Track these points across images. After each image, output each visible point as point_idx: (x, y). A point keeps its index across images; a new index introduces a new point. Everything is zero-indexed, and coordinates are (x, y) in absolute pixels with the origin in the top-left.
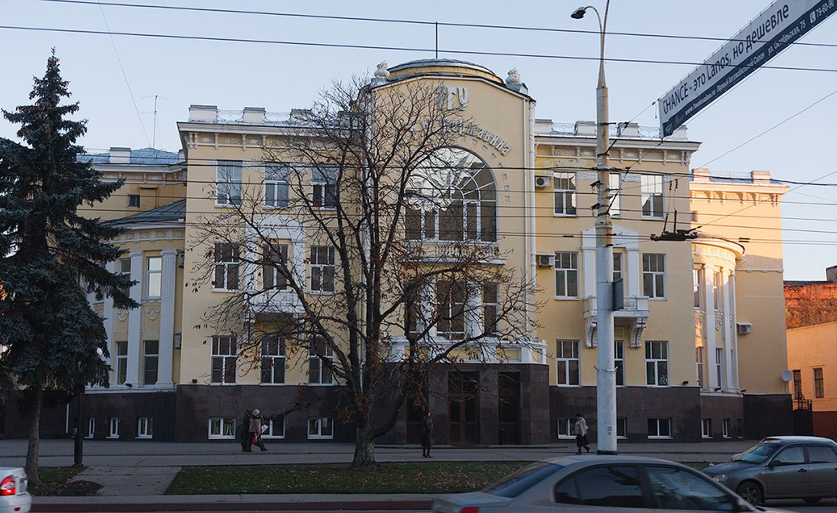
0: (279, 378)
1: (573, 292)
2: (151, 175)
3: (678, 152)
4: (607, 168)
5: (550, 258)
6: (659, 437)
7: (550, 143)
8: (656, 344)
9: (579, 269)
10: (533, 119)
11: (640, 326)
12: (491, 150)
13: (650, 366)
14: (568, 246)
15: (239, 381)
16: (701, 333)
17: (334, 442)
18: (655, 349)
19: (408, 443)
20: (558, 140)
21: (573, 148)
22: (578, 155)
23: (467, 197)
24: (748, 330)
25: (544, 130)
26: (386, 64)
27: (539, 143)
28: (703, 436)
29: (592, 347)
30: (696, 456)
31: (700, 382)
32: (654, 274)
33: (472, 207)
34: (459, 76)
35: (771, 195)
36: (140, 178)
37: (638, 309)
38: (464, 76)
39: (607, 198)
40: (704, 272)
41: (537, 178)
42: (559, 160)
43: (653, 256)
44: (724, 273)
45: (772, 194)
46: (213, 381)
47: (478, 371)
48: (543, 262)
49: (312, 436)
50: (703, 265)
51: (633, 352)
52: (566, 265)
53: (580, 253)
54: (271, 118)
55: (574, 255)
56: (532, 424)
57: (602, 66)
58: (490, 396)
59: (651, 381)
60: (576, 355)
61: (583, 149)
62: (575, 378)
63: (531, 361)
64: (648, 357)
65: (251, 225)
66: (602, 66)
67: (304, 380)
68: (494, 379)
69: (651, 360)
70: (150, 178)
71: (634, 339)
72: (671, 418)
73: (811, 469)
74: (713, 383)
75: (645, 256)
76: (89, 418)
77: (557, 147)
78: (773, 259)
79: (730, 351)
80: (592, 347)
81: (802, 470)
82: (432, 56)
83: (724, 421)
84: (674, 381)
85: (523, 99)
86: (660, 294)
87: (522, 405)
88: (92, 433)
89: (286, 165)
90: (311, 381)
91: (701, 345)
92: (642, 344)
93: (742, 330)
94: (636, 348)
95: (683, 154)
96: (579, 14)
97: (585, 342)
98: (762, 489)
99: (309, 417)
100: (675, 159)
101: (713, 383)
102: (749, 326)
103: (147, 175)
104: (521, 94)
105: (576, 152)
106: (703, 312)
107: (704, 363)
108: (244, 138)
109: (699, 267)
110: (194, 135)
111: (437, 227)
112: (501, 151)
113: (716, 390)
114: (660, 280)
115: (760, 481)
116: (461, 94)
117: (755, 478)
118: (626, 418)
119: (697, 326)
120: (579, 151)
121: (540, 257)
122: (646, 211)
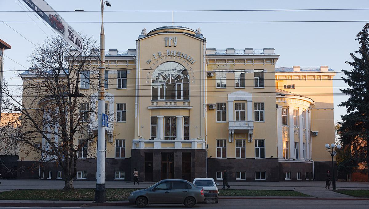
0: (263, 155)
1: (224, 119)
3: (270, 59)
4: (102, 67)
5: (213, 106)
6: (260, 179)
7: (214, 58)
8: (260, 140)
9: (246, 110)
10: (205, 49)
11: (250, 133)
12: (187, 62)
13: (257, 150)
14: (222, 100)
15: (228, 157)
16: (287, 136)
17: (266, 181)
18: (260, 143)
19: (145, 181)
21: (225, 60)
22: (227, 63)
23: (178, 82)
24: (317, 134)
25: (213, 53)
26: (146, 29)
27: (208, 58)
29: (231, 142)
30: (287, 187)
32: (259, 111)
33: (179, 86)
34: (174, 33)
35: (329, 76)
37: (249, 126)
38: (176, 33)
39: (102, 80)
40: (289, 110)
41: (208, 73)
43: (259, 104)
44: (300, 110)
45: (320, 75)
46: (116, 157)
48: (210, 107)
49: (218, 178)
50: (288, 107)
51: (249, 144)
52: (221, 108)
53: (227, 103)
54: (236, 52)
55: (225, 104)
56: (196, 174)
58: (178, 162)
59: (238, 156)
60: (225, 145)
61: (228, 60)
62: (224, 154)
63: (196, 148)
64: (256, 146)
65: (9, 95)
68: (180, 155)
71: (250, 138)
73: (171, 192)
74: (292, 156)
75: (255, 104)
76: (57, 171)
77: (217, 60)
78: (329, 104)
79: (294, 144)
80: (231, 142)
81: (167, 192)
82: (171, 25)
83: (306, 173)
84: (267, 156)
85: (200, 40)
86: (262, 119)
87: (191, 166)
88: (50, 177)
90: (116, 157)
91: (287, 141)
92: (253, 141)
93: (314, 135)
94: (251, 142)
95: (272, 60)
96: (108, 4)
97: (228, 140)
98: (147, 200)
99: (236, 171)
100: (269, 63)
101: (292, 156)
102: (317, 132)
104: (200, 39)
105: (226, 61)
106: (288, 127)
107: (288, 148)
108: (254, 60)
109: (286, 108)
111: (165, 94)
112: (192, 62)
114: (262, 113)
115: (195, 198)
116: (174, 39)
117: (145, 195)
118: (290, 172)
119: (285, 133)
120: (117, 62)
121: (209, 106)
122: (237, 85)
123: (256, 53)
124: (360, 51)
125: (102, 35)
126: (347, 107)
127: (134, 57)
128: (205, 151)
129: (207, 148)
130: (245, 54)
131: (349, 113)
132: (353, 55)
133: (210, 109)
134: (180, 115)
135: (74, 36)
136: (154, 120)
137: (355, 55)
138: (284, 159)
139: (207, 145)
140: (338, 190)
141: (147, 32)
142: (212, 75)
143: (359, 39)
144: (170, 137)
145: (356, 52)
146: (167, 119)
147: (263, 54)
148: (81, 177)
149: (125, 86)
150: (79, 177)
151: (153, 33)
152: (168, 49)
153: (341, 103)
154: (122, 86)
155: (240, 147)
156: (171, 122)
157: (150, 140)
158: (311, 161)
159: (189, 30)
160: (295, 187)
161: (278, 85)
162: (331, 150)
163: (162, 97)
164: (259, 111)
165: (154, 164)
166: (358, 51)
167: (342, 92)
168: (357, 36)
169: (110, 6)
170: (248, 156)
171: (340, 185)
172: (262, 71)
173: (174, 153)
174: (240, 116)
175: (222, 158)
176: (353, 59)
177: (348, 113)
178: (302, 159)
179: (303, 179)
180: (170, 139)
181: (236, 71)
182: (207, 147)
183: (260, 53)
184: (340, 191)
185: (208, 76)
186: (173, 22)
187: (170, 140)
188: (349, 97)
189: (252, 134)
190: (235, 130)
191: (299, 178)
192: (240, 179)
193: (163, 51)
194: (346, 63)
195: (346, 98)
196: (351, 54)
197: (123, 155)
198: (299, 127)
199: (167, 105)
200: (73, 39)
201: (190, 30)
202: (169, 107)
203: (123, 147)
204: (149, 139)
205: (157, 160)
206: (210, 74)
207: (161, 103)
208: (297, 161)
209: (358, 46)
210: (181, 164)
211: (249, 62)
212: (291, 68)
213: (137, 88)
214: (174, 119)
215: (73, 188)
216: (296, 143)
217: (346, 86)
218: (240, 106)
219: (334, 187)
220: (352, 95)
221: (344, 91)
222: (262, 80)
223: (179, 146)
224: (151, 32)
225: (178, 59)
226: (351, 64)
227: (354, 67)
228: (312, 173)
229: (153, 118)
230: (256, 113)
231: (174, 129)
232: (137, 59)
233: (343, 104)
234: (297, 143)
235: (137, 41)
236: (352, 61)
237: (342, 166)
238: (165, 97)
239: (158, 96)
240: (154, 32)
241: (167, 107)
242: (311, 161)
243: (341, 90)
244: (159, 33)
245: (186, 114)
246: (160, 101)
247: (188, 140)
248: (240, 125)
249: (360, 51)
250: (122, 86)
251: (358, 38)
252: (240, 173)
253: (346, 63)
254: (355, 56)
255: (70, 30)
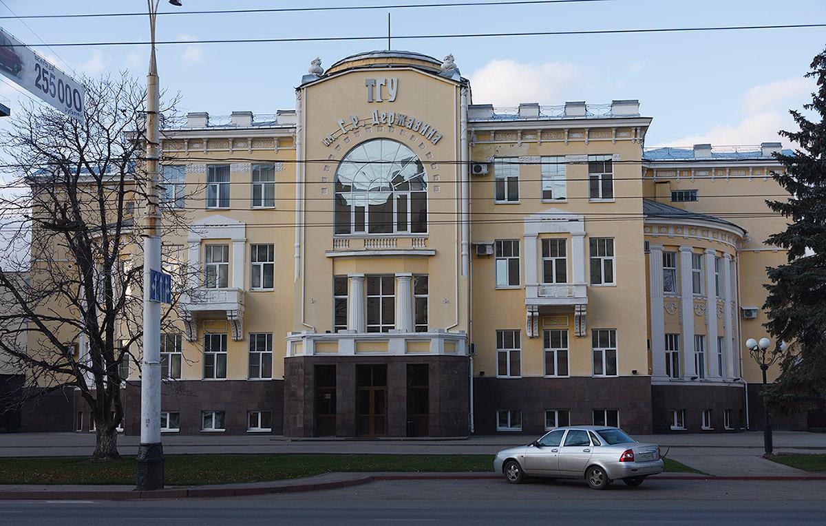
0: (563, 369)
2: (698, 171)
5: (487, 247)
6: (509, 429)
13: (668, 355)
20: (569, 122)
28: (704, 427)
29: (532, 337)
31: (650, 372)
32: (603, 259)
36: (674, 173)
38: (392, 67)
41: (474, 166)
42: (500, 145)
46: (206, 377)
47: (386, 363)
54: (544, 113)
57: (153, 48)
66: (153, 48)
67: (244, 376)
69: (551, 349)
70: (697, 173)
72: (684, 410)
80: (532, 337)
82: (382, 46)
89: (164, 160)
90: (251, 376)
99: (545, 410)
101: (688, 367)
103: (695, 171)
110: (636, 130)
113: (693, 378)
114: (609, 264)
123: (594, 112)
124: (817, 104)
125: (153, 75)
126: (786, 246)
127: (290, 130)
128: (465, 360)
129: (473, 352)
130: (566, 116)
131: (792, 261)
132: (797, 115)
133: (478, 255)
134: (402, 272)
135: (56, 82)
136: (341, 285)
137: (801, 115)
138: (668, 379)
139: (473, 345)
140: (780, 455)
141: (325, 66)
142: (484, 170)
143: (814, 73)
144: (381, 325)
145: (806, 107)
146: (371, 282)
147: (612, 115)
148: (258, 427)
149: (225, 201)
150: (504, 422)
151: (338, 69)
152: (375, 108)
153: (772, 236)
154: (218, 201)
155: (555, 350)
156: (379, 286)
157: (329, 334)
158: (739, 383)
159: (427, 59)
160: (669, 446)
161: (655, 194)
162: (761, 355)
163: (360, 227)
164: (603, 259)
165: (339, 394)
166: (812, 105)
167: (771, 210)
168: (812, 66)
169: (180, 5)
170: (572, 372)
171: (785, 441)
172: (607, 158)
173: (387, 365)
174: (555, 272)
175: (559, 377)
176: (798, 124)
177: (789, 260)
178: (713, 377)
179: (718, 429)
180: (381, 331)
181: (545, 160)
182: (472, 348)
183: (558, 113)
184: (783, 459)
185: (474, 172)
186: (389, 38)
187: (381, 334)
188: (790, 220)
189: (584, 316)
190: (541, 308)
191: (707, 425)
192: (259, 429)
193: (368, 113)
194: (780, 134)
195: (782, 223)
196: (791, 112)
197: (267, 372)
198: (681, 295)
199: (379, 246)
200: (51, 87)
201: (430, 60)
202: (377, 253)
203: (266, 352)
204: (327, 332)
205: (397, 386)
206: (478, 169)
207: (358, 241)
208: (701, 381)
209: (813, 87)
210: (404, 392)
211: (575, 135)
212: (688, 149)
213: (464, 202)
214: (389, 282)
215: (118, 453)
216: (700, 338)
217: (784, 196)
218: (553, 247)
219: (769, 446)
220: (797, 216)
221: (776, 206)
222: (608, 181)
223: (396, 348)
224: (333, 67)
225: (396, 132)
226: (792, 137)
227: (802, 146)
228: (742, 412)
229: (558, 279)
230: (595, 265)
231: (390, 306)
232: (297, 135)
233: (777, 239)
234: (702, 337)
235: (298, 89)
236: (796, 128)
237: (770, 393)
238: (367, 228)
239: (364, 226)
240: (342, 70)
241: (372, 253)
242: (739, 383)
243: (770, 204)
244: (351, 69)
245: (419, 268)
246: (355, 238)
247: (425, 333)
248: (557, 294)
249: (817, 104)
250: (218, 201)
251: (812, 70)
252: (554, 412)
253: (780, 134)
254: (802, 118)
255: (42, 66)
